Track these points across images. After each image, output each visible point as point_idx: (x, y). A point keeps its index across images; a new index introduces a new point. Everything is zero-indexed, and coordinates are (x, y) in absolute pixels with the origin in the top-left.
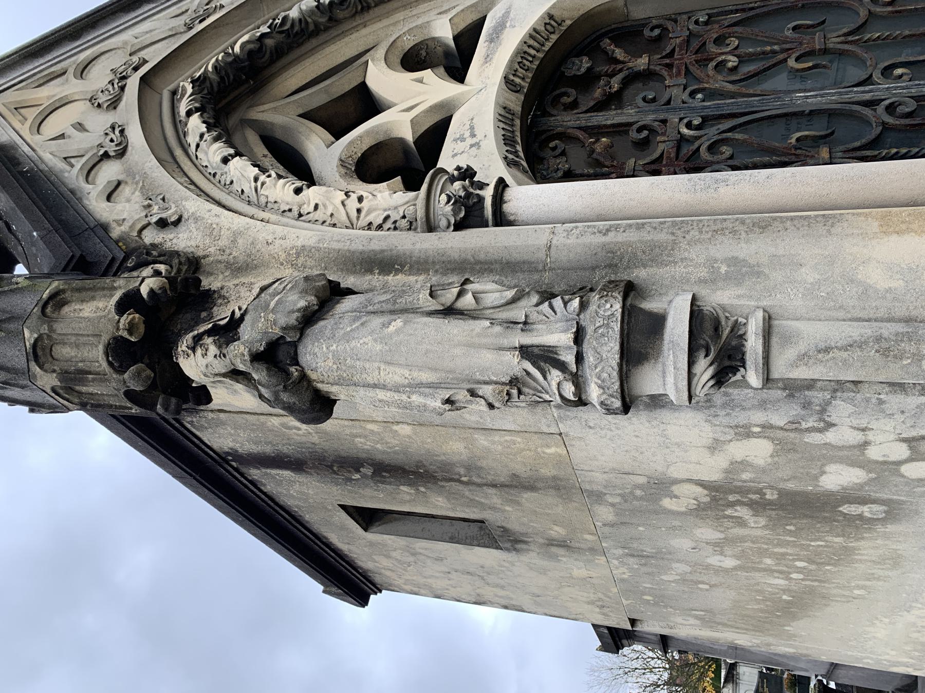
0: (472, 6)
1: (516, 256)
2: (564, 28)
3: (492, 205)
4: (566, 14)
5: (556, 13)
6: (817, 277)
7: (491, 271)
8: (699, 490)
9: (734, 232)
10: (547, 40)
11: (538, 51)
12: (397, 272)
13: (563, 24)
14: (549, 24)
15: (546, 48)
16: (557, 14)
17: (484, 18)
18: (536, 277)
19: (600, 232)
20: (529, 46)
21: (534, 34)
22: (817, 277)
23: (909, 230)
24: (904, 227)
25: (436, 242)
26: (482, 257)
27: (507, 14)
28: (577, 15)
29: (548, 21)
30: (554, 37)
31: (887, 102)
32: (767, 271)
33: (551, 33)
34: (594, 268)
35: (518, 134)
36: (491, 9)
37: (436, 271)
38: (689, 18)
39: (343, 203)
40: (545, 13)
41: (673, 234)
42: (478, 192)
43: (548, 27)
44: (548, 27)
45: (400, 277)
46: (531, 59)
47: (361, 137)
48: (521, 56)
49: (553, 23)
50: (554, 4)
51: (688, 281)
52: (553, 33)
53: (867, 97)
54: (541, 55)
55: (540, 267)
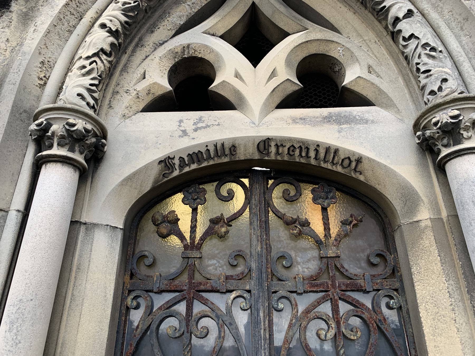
0: (380, 90)
2: (354, 176)
4: (369, 174)
5: (365, 162)
10: (333, 163)
11: (316, 158)
13: (358, 174)
14: (351, 162)
15: (323, 165)
16: (365, 165)
17: (375, 105)
20: (317, 151)
21: (332, 151)
28: (373, 183)
29: (353, 159)
30: (339, 169)
33: (342, 164)
35: (211, 162)
36: (382, 107)
38: (396, 290)
39: (81, 57)
43: (347, 162)
44: (347, 162)
46: (304, 154)
47: (213, 51)
48: (304, 146)
49: (354, 164)
50: (374, 161)
52: (343, 167)
54: (313, 162)
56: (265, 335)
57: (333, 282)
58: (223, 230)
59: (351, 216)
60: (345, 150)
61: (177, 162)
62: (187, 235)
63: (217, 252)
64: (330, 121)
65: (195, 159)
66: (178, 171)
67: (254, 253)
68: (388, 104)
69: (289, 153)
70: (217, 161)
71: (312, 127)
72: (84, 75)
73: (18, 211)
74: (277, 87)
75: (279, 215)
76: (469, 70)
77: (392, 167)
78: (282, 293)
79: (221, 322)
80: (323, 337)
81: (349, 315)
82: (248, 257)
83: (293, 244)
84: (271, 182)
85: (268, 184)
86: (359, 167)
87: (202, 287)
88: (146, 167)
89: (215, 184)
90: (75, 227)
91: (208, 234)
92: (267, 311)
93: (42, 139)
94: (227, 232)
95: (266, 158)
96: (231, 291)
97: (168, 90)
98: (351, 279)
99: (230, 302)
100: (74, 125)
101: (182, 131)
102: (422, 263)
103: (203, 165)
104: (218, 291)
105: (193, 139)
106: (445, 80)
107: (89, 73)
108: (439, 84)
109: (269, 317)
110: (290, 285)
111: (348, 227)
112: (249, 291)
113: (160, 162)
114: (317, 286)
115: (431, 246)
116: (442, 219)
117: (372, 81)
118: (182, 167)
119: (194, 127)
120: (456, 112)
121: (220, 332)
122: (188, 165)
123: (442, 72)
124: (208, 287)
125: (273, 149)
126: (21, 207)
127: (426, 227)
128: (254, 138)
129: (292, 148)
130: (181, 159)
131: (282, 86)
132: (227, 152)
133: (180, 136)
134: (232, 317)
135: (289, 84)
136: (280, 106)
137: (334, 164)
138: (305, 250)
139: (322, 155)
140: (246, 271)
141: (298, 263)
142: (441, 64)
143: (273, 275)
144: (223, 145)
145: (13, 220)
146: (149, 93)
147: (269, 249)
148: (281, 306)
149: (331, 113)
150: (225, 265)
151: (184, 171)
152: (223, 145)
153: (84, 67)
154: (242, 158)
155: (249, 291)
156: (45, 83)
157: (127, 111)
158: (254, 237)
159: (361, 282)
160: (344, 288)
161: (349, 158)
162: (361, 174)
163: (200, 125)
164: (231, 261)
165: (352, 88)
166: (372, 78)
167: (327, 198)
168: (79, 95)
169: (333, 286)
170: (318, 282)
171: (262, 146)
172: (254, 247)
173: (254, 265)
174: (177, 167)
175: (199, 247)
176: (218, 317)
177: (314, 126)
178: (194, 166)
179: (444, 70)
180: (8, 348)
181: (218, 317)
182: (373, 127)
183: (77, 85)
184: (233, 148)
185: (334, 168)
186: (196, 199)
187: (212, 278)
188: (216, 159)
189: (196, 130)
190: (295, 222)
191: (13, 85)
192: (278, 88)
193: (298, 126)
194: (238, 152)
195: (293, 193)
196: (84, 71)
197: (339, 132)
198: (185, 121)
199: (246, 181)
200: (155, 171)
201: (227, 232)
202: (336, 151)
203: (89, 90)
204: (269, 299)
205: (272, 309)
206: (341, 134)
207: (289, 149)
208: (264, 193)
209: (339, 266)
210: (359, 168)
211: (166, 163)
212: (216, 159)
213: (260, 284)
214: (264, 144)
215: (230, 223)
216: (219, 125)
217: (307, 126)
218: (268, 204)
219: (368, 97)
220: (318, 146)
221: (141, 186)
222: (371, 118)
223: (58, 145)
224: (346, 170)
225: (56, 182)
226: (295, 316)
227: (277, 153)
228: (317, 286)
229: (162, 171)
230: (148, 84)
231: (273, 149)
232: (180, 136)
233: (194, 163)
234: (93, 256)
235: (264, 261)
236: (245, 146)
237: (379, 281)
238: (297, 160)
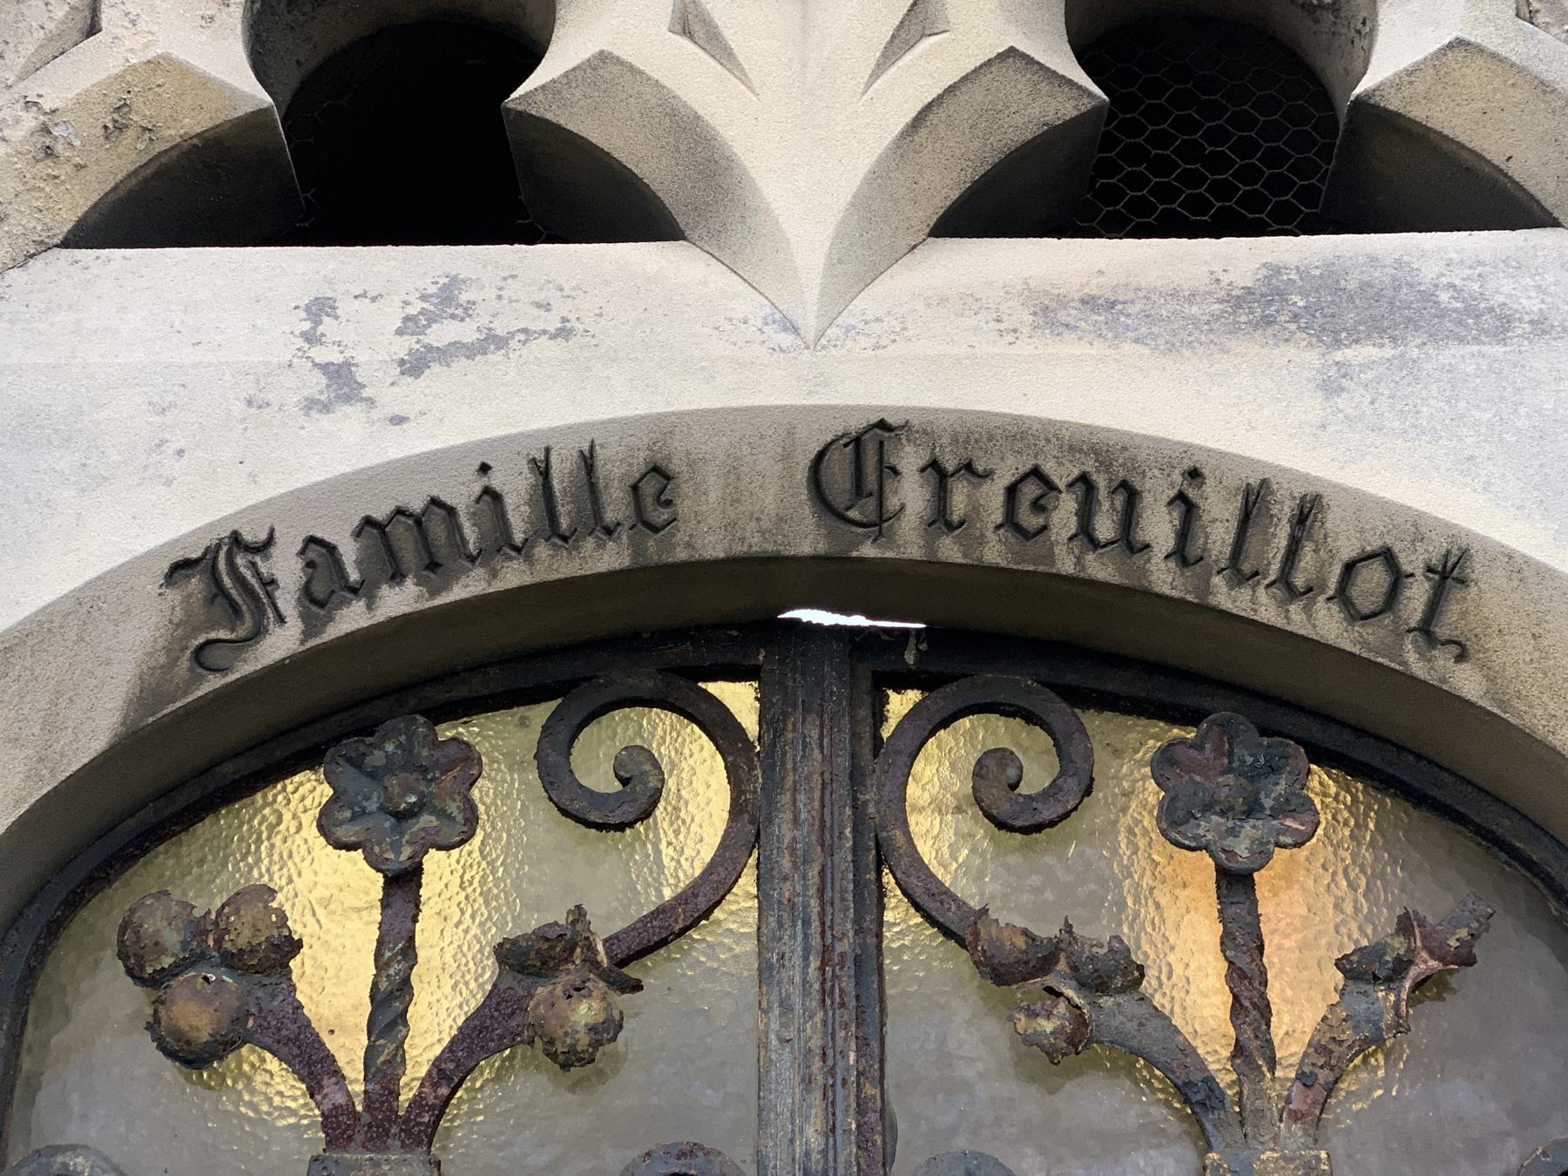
2: (1418, 669)
4: (1512, 654)
5: (1487, 583)
11: (1182, 554)
13: (1443, 659)
14: (1398, 578)
15: (1224, 596)
16: (1484, 604)
20: (1186, 506)
21: (1284, 511)
27: (1490, 323)
30: (1325, 624)
33: (1342, 596)
35: (513, 575)
44: (1373, 580)
46: (1105, 528)
48: (1107, 480)
49: (1417, 596)
52: (1354, 615)
54: (1164, 578)
58: (585, 1012)
59: (1405, 925)
60: (1361, 502)
61: (286, 568)
62: (349, 1050)
64: (1268, 321)
65: (402, 536)
69: (1010, 521)
70: (551, 565)
75: (950, 917)
83: (1030, 1102)
85: (879, 717)
88: (88, 605)
89: (541, 713)
95: (868, 551)
97: (244, 110)
101: (325, 368)
103: (458, 592)
105: (398, 420)
113: (180, 569)
117: (1539, 68)
118: (316, 603)
119: (404, 346)
128: (788, 419)
129: (1030, 490)
130: (318, 551)
132: (616, 506)
133: (310, 405)
135: (1016, 83)
136: (962, 220)
137: (1292, 593)
139: (1218, 533)
144: (588, 462)
146: (120, 128)
149: (1277, 270)
152: (588, 462)
154: (713, 547)
158: (785, 1065)
162: (1461, 657)
163: (442, 334)
165: (1417, 113)
167: (1252, 809)
174: (287, 600)
177: (1171, 348)
178: (399, 600)
184: (657, 482)
185: (1296, 620)
188: (542, 551)
189: (414, 366)
190: (1045, 964)
192: (951, 105)
193: (1070, 347)
194: (684, 507)
195: (1038, 774)
197: (1330, 388)
198: (345, 307)
200: (142, 632)
202: (1308, 513)
206: (1342, 401)
207: (1012, 491)
208: (856, 777)
212: (542, 551)
214: (856, 461)
216: (564, 333)
217: (1128, 348)
218: (880, 849)
219: (1516, 171)
220: (1194, 474)
221: (51, 726)
222: (1531, 304)
227: (940, 519)
229: (187, 625)
230: (114, 66)
232: (310, 405)
233: (397, 577)
236: (733, 471)
238: (1066, 566)
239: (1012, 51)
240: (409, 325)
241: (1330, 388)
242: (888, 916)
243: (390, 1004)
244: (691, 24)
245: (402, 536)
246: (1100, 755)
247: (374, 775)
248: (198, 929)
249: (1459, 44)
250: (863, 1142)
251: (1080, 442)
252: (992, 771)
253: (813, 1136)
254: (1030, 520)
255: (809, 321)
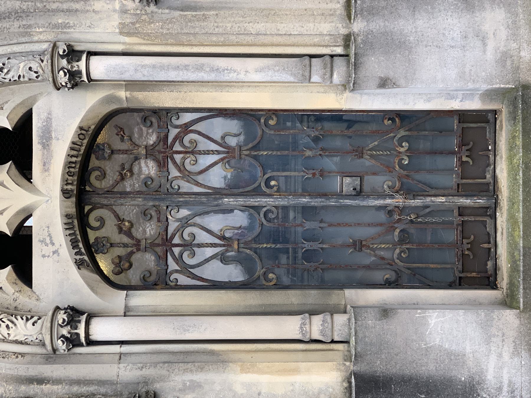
1: (103, 378)
2: (91, 132)
3: (85, 341)
4: (90, 122)
6: (220, 388)
7: (93, 384)
8: (233, 126)
9: (191, 371)
11: (77, 157)
12: (46, 384)
13: (90, 129)
14: (81, 134)
15: (82, 152)
16: (84, 125)
18: (114, 387)
19: (139, 368)
20: (72, 156)
21: (73, 146)
22: (220, 388)
23: (249, 372)
24: (248, 370)
25: (64, 371)
26: (88, 378)
27: (49, 120)
30: (85, 141)
31: (265, 209)
32: (203, 385)
33: (83, 140)
34: (138, 383)
35: (78, 232)
36: (34, 104)
37: (66, 383)
40: (77, 128)
41: (168, 371)
42: (76, 331)
44: (81, 136)
45: (48, 386)
46: (74, 165)
48: (68, 165)
49: (83, 132)
50: (82, 119)
51: (175, 390)
52: (84, 139)
53: (257, 204)
54: (79, 159)
55: (115, 383)
56: (193, 198)
57: (162, 152)
58: (127, 224)
59: (117, 135)
60: (73, 137)
61: (78, 257)
62: (129, 250)
63: (141, 229)
64: (48, 145)
65: (75, 244)
66: (84, 256)
67: (142, 203)
68: (34, 99)
70: (77, 228)
71: (52, 160)
72: (15, 325)
73: (121, 347)
74: (15, 182)
75: (115, 184)
76: (21, 47)
77: (88, 108)
78: (168, 186)
79: (186, 225)
80: (194, 162)
81: (182, 144)
82: (145, 207)
83: (135, 176)
84: (88, 188)
85: (89, 191)
86: (85, 128)
87: (165, 237)
88: (83, 278)
89: (88, 230)
90: (127, 313)
91: (129, 234)
92: (180, 196)
93: (73, 341)
94: (129, 222)
95: (75, 192)
96: (167, 218)
97: (11, 269)
98: (160, 141)
99: (174, 219)
100: (64, 320)
101: (53, 254)
102: (152, 101)
103: (80, 239)
104: (167, 227)
105: (61, 245)
106: (30, 69)
107: (12, 322)
108: (33, 73)
109: (183, 194)
110: (163, 181)
111: (125, 138)
112: (167, 207)
113: (79, 268)
114: (164, 163)
115: (143, 94)
116: (126, 84)
117: (11, 109)
118: (81, 254)
119: (50, 246)
120: (61, 73)
121: (191, 226)
122: (80, 249)
123: (23, 69)
124: (164, 233)
125: (69, 187)
126: (118, 346)
127: (130, 94)
128: (61, 201)
129: (69, 174)
130: (76, 254)
131: (12, 177)
132: (70, 221)
133: (58, 255)
134: (183, 218)
135: (11, 172)
137: (82, 145)
138: (140, 168)
139: (75, 153)
140: (154, 208)
141: (149, 173)
142: (15, 68)
143: (157, 191)
144: (65, 224)
145: (125, 349)
146: (15, 283)
147: (139, 193)
148: (176, 187)
149: (39, 143)
150: (150, 223)
151: (84, 252)
152: (65, 224)
153: (7, 326)
154: (74, 210)
155: (167, 207)
156: (20, 354)
157: (33, 298)
158: (132, 203)
159: (162, 135)
160: (166, 146)
161: (79, 135)
162: (90, 127)
163: (48, 241)
164: (148, 218)
165: (15, 123)
166: (8, 108)
167: (104, 150)
168: (33, 325)
169: (165, 152)
170: (162, 162)
171: (67, 195)
172: (139, 203)
173: (151, 203)
174: (82, 257)
175: (139, 241)
176: (182, 227)
177: (52, 157)
178: (81, 245)
179: (21, 67)
180: (197, 329)
181: (182, 227)
182: (54, 115)
183: (23, 329)
184: (68, 216)
185: (85, 145)
186: (103, 244)
187: (159, 231)
188: (75, 229)
189: (53, 244)
190: (121, 174)
191: (29, 369)
192: (15, 180)
193: (52, 168)
194: (70, 213)
195: (97, 173)
196: (11, 325)
197: (58, 139)
198: (43, 253)
199: (87, 208)
200: (85, 272)
201: (129, 222)
202: (73, 143)
203: (27, 320)
204: (172, 194)
205: (179, 194)
206: (60, 138)
207: (69, 176)
208: (98, 194)
209: (152, 148)
210: (86, 129)
211: (79, 264)
212: (75, 229)
213: (163, 200)
214: (65, 193)
215: (122, 219)
216: (48, 227)
217: (52, 162)
218: (109, 192)
219: (24, 112)
220: (68, 155)
221: (96, 281)
222: (46, 114)
223: (76, 329)
224: (87, 137)
225: (100, 329)
226: (182, 178)
227: (71, 184)
228: (164, 163)
229: (85, 268)
230: (8, 285)
231: (69, 187)
232: (58, 255)
233: (78, 245)
234: (147, 304)
235: (148, 196)
236: (66, 207)
237: (162, 124)
238: (77, 170)
239: (7, 173)
240: (47, 245)
241: (58, 139)
242: (128, 190)
243: (125, 246)
244: (0, 213)
245: (75, 244)
246: (95, 166)
247: (98, 249)
248: (117, 266)
249: (7, 118)
250: (140, 194)
251: (64, 168)
252: (97, 178)
253: (140, 199)
254: (72, 173)
255: (48, 198)
